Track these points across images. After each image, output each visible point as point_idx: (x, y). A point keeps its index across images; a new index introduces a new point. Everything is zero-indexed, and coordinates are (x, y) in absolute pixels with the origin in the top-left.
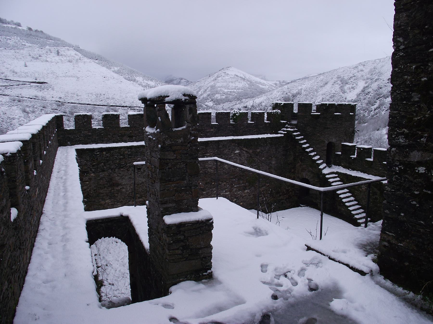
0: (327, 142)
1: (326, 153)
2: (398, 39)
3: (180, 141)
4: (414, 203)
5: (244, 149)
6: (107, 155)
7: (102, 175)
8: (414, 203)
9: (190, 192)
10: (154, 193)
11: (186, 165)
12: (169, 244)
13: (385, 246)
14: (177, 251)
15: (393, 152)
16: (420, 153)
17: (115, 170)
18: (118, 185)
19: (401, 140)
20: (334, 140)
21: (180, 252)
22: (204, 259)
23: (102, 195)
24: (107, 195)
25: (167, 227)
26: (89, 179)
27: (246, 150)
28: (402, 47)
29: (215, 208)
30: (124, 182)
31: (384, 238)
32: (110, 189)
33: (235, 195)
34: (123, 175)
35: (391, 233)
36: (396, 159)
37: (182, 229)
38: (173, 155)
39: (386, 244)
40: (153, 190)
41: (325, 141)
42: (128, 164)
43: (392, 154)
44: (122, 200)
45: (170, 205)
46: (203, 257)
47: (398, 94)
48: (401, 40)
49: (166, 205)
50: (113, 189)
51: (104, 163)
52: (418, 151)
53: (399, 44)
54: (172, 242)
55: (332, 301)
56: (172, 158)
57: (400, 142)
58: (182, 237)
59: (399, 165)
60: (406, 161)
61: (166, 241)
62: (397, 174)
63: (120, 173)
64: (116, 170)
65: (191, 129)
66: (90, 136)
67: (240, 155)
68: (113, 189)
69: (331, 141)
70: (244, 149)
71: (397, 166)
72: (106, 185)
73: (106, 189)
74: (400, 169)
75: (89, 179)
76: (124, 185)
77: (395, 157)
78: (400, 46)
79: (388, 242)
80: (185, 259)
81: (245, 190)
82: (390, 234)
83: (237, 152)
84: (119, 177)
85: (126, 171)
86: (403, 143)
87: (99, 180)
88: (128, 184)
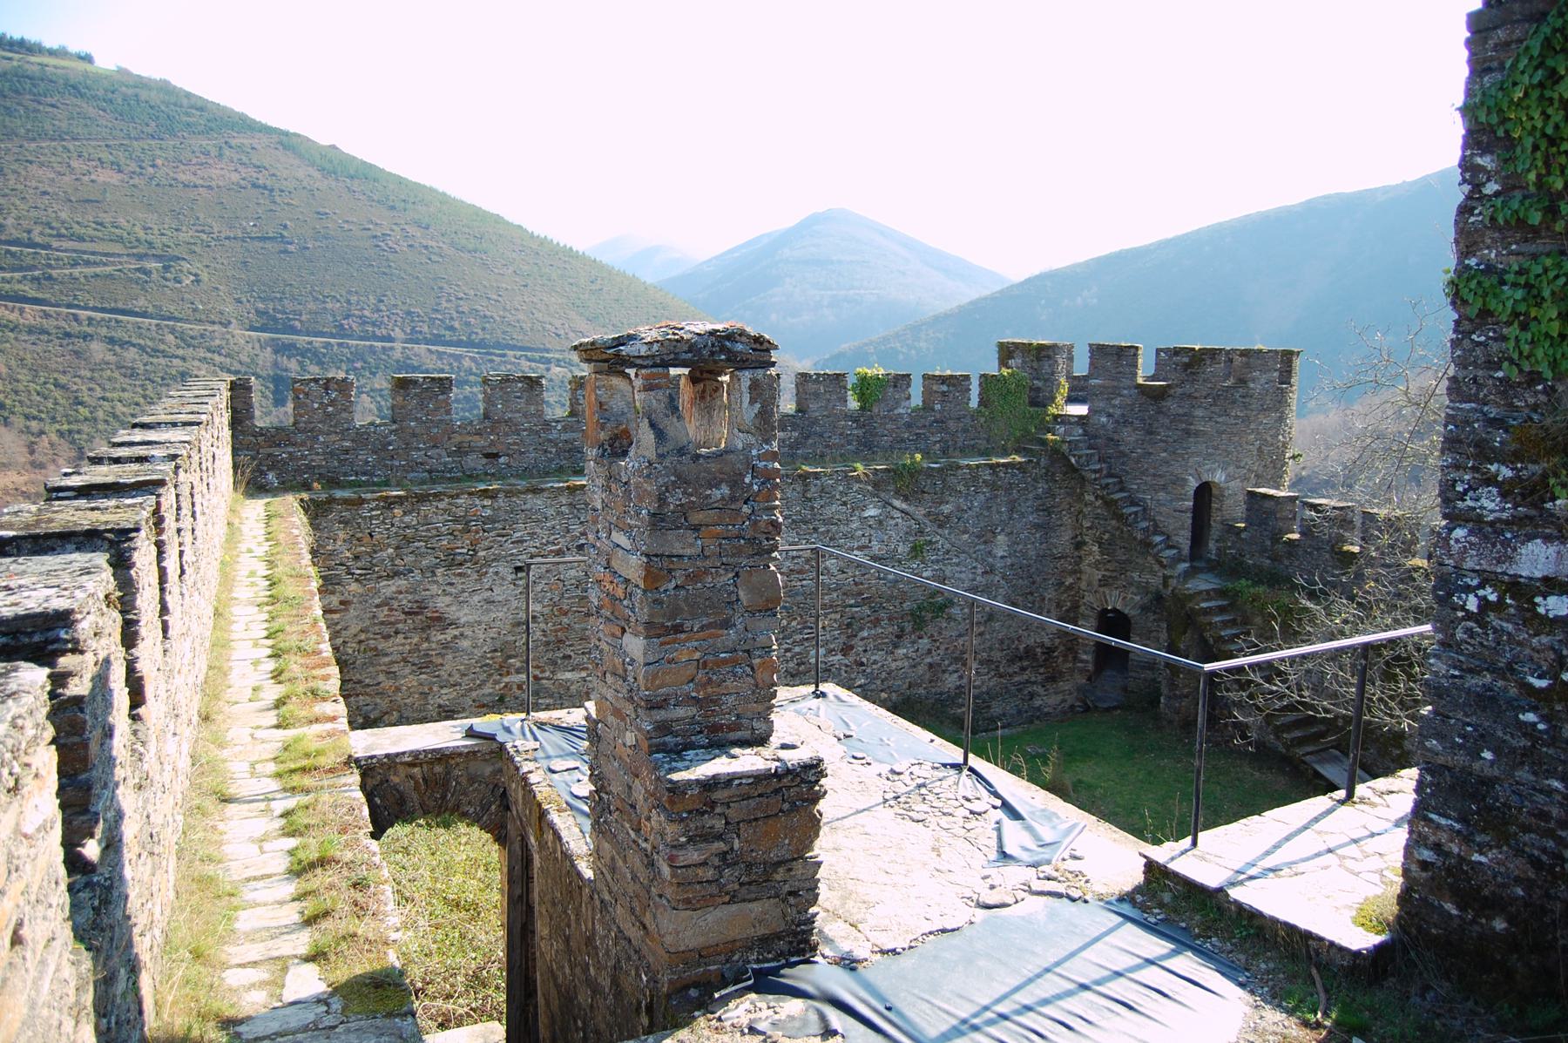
0: (1193, 484)
1: (1190, 521)
2: (1479, 160)
3: (717, 494)
4: (1530, 717)
5: (897, 503)
6: (407, 519)
7: (389, 588)
8: (1530, 717)
9: (748, 669)
10: (621, 672)
11: (737, 575)
12: (674, 847)
13: (1424, 865)
14: (700, 871)
15: (1457, 541)
16: (1552, 550)
17: (434, 574)
18: (440, 622)
19: (1485, 503)
20: (1219, 477)
21: (710, 874)
22: (792, 900)
23: (387, 659)
24: (405, 660)
25: (669, 790)
26: (341, 603)
27: (904, 506)
28: (1491, 188)
29: (813, 723)
30: (464, 615)
31: (1420, 834)
32: (416, 640)
33: (862, 664)
34: (463, 591)
35: (1447, 817)
36: (1469, 564)
37: (719, 795)
38: (691, 540)
39: (1427, 855)
40: (618, 661)
41: (1186, 480)
42: (482, 554)
43: (1456, 547)
44: (457, 677)
45: (681, 712)
46: (790, 893)
47: (1479, 344)
48: (1485, 161)
49: (663, 712)
50: (427, 639)
51: (397, 548)
52: (1548, 539)
53: (1482, 177)
54: (683, 839)
55: (83, 846)
56: (688, 552)
57: (1482, 508)
58: (719, 824)
59: (1481, 586)
60: (1504, 573)
61: (662, 834)
62: (1469, 616)
63: (451, 584)
64: (439, 571)
65: (754, 452)
66: (347, 452)
67: (880, 522)
68: (427, 639)
69: (1206, 477)
70: (897, 503)
71: (1468, 589)
72: (400, 626)
73: (400, 639)
74: (1483, 601)
75: (341, 603)
76: (469, 624)
77: (1463, 559)
78: (1484, 184)
79: (1437, 847)
80: (727, 898)
81: (896, 646)
82: (1443, 821)
83: (872, 512)
84: (448, 599)
85: (475, 576)
86: (1492, 511)
87: (377, 606)
88: (479, 623)
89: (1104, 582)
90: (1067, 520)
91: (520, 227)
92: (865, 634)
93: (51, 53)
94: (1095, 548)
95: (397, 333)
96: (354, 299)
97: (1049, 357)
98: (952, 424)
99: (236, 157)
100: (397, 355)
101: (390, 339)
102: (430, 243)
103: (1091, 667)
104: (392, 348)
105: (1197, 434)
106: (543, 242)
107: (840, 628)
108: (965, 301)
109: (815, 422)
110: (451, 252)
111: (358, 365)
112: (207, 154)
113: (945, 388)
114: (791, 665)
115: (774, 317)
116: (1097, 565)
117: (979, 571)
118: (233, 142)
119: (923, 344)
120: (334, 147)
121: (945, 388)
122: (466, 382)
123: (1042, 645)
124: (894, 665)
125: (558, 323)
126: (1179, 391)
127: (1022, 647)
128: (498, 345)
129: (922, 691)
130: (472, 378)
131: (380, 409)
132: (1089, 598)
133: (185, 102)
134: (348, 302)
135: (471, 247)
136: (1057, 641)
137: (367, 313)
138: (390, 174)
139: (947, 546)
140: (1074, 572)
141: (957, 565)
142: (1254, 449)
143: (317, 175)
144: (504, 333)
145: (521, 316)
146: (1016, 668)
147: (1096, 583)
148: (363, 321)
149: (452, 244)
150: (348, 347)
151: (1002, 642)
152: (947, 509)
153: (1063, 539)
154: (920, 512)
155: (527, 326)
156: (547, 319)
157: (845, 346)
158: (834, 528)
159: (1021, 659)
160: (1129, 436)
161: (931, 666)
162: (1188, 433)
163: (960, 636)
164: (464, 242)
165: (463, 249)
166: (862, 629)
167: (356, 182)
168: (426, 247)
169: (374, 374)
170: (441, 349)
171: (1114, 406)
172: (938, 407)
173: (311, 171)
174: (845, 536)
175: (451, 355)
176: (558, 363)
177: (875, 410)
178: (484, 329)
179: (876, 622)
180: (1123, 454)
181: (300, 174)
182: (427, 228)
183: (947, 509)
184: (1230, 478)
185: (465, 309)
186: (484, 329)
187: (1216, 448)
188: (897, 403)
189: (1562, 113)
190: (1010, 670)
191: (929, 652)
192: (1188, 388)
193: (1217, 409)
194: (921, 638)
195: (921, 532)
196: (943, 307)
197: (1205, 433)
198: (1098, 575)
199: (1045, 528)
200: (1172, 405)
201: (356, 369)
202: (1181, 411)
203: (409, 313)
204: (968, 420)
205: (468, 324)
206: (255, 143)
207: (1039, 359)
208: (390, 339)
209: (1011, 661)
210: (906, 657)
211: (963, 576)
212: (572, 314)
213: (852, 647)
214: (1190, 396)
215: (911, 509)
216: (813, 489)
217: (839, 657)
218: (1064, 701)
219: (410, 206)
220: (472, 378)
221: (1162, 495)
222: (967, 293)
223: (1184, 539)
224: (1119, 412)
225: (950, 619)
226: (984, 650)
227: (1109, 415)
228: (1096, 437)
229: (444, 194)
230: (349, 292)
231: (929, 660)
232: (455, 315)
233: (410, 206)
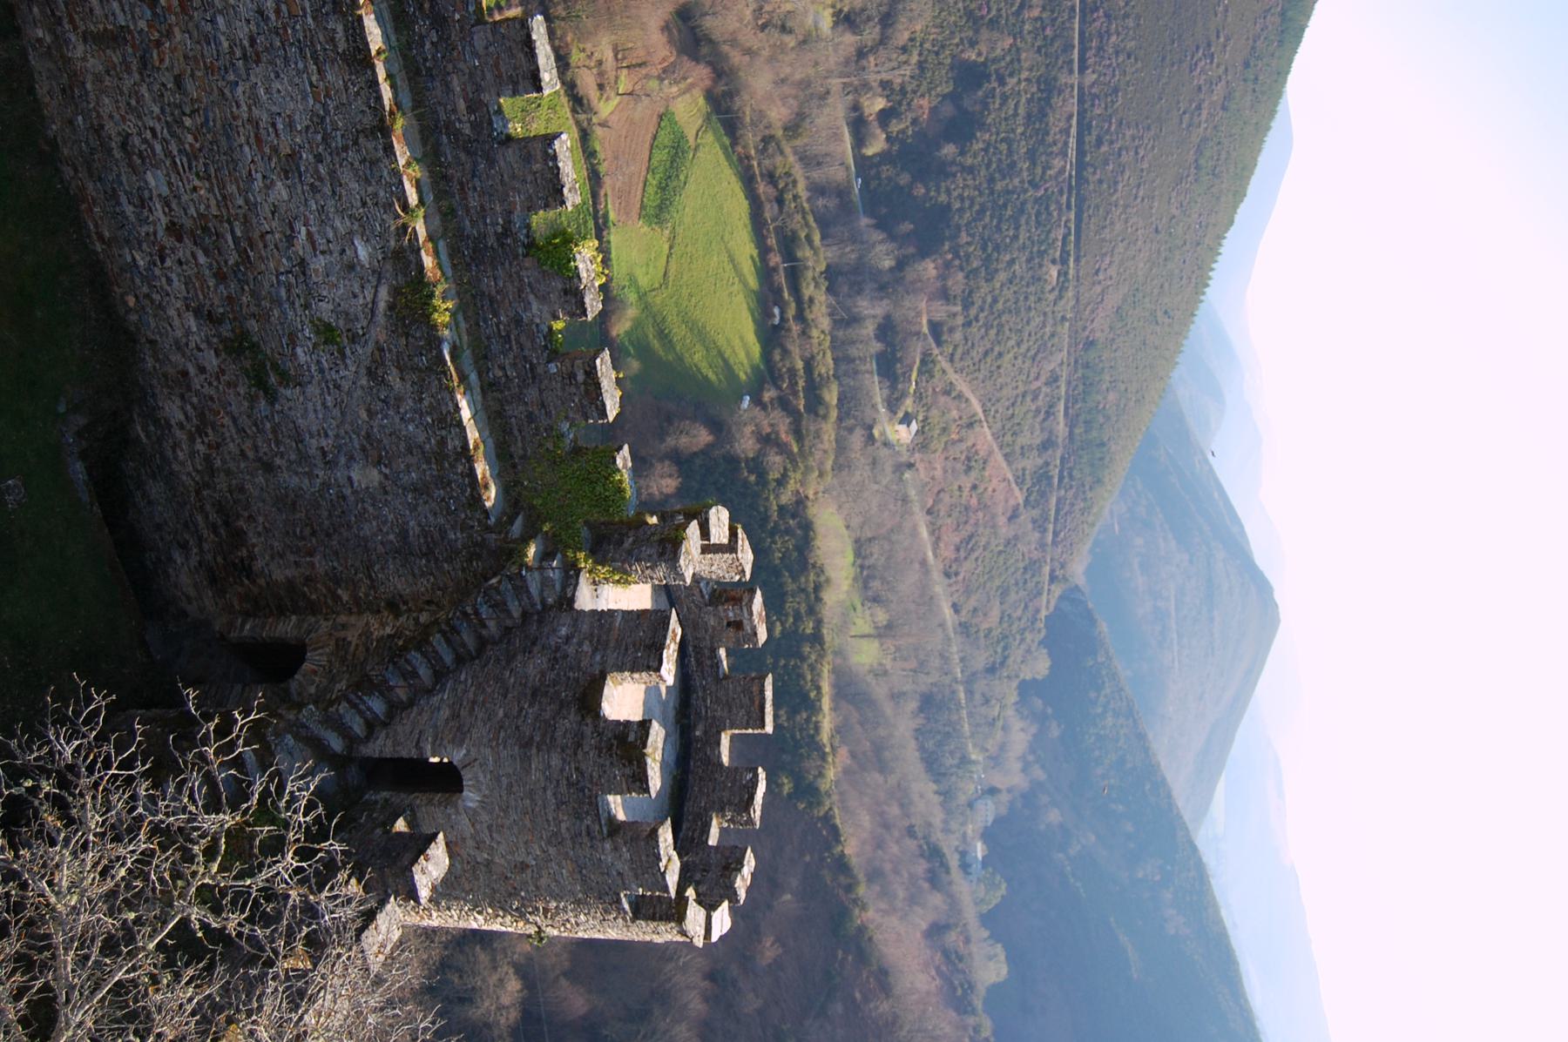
1: (404, 754)
5: (384, 293)
20: (471, 797)
27: (382, 305)
69: (467, 777)
81: (197, 313)
83: (363, 252)
89: (342, 644)
90: (424, 584)
91: (1231, 222)
92: (202, 259)
94: (388, 630)
95: (1090, 77)
96: (1130, 23)
97: (661, 554)
98: (532, 394)
100: (1063, 79)
101: (1083, 68)
102: (1204, 113)
103: (234, 635)
104: (1071, 72)
105: (526, 759)
106: (1214, 251)
107: (201, 216)
108: (1169, 777)
109: (491, 162)
110: (1195, 139)
111: (1048, 32)
113: (581, 377)
114: (137, 141)
115: (1139, 541)
116: (366, 634)
117: (324, 443)
119: (1110, 721)
121: (581, 377)
122: (1034, 163)
123: (252, 558)
124: (172, 312)
125: (1112, 271)
126: (588, 730)
127: (241, 523)
128: (1081, 201)
129: (150, 363)
130: (1039, 170)
131: (995, 61)
132: (325, 626)
134: (1126, 16)
135: (1202, 162)
136: (262, 581)
137: (1114, 38)
138: (1290, 61)
139: (346, 385)
140: (357, 600)
141: (324, 404)
142: (520, 857)
144: (1097, 207)
145: (1118, 227)
146: (213, 516)
147: (342, 634)
148: (1103, 36)
149: (1204, 140)
150: (1071, 18)
151: (242, 489)
152: (393, 377)
153: (396, 581)
154: (379, 333)
155: (1106, 234)
156: (1117, 259)
157: (1104, 627)
158: (327, 190)
159: (227, 524)
160: (534, 667)
161: (185, 374)
162: (526, 744)
163: (234, 420)
164: (1208, 154)
165: (1199, 151)
166: (206, 253)
167: (1278, 20)
168: (1199, 108)
169: (1039, 51)
170: (1074, 131)
171: (580, 644)
172: (553, 368)
174: (322, 210)
175: (1066, 143)
176: (1063, 274)
177: (528, 262)
178: (1100, 182)
179: (221, 277)
180: (510, 658)
182: (1224, 108)
183: (393, 377)
184: (473, 816)
185: (1124, 158)
186: (1100, 182)
187: (510, 792)
188: (543, 299)
190: (208, 507)
191: (202, 370)
192: (590, 741)
193: (563, 788)
194: (217, 355)
195: (354, 339)
196: (1161, 746)
197: (528, 772)
198: (352, 636)
199: (403, 550)
200: (569, 721)
201: (1044, 29)
202: (559, 734)
203: (1116, 90)
204: (545, 422)
205: (1106, 163)
207: (661, 541)
208: (1083, 68)
209: (220, 508)
210: (188, 332)
211: (312, 415)
212: (1124, 289)
213: (180, 240)
214: (579, 745)
215: (380, 318)
216: (370, 145)
217: (164, 220)
218: (189, 599)
219: (1251, 85)
220: (1039, 170)
221: (445, 713)
222: (1178, 779)
223: (380, 747)
224: (571, 650)
225: (253, 399)
226: (224, 462)
227: (568, 639)
228: (540, 622)
229: (1268, 128)
230: (1138, 17)
231: (192, 370)
232: (1117, 146)
233: (1251, 85)
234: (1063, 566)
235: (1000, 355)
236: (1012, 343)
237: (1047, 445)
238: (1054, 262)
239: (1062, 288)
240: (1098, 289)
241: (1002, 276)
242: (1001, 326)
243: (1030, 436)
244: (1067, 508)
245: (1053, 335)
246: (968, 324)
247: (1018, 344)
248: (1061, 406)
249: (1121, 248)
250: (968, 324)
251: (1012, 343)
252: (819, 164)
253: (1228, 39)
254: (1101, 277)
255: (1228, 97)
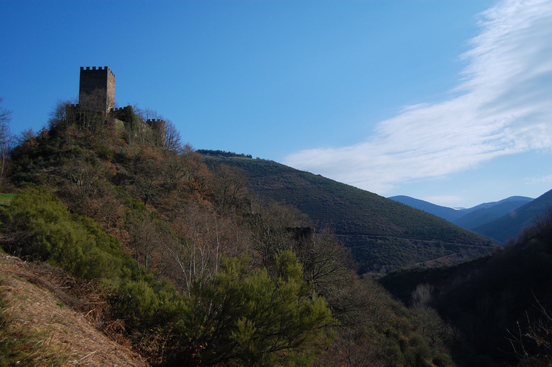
93: (238, 155)
99: (283, 180)
112: (274, 180)
118: (284, 176)
120: (320, 175)
125: (384, 226)
133: (271, 165)
143: (309, 184)
168: (340, 204)
173: (307, 183)
176: (381, 239)
178: (355, 229)
181: (303, 184)
189: (415, 296)
205: (350, 227)
206: (291, 176)
234: (484, 242)
235: (402, 256)
236: (399, 253)
237: (438, 245)
238: (377, 241)
239: (385, 239)
240: (388, 230)
241: (377, 254)
242: (393, 256)
243: (434, 250)
244: (462, 241)
245: (400, 242)
246: (390, 264)
247: (400, 251)
248: (426, 241)
249: (377, 224)
250: (390, 264)
251: (399, 253)
252: (31, 349)
253: (323, 197)
254: (385, 229)
255: (341, 197)
